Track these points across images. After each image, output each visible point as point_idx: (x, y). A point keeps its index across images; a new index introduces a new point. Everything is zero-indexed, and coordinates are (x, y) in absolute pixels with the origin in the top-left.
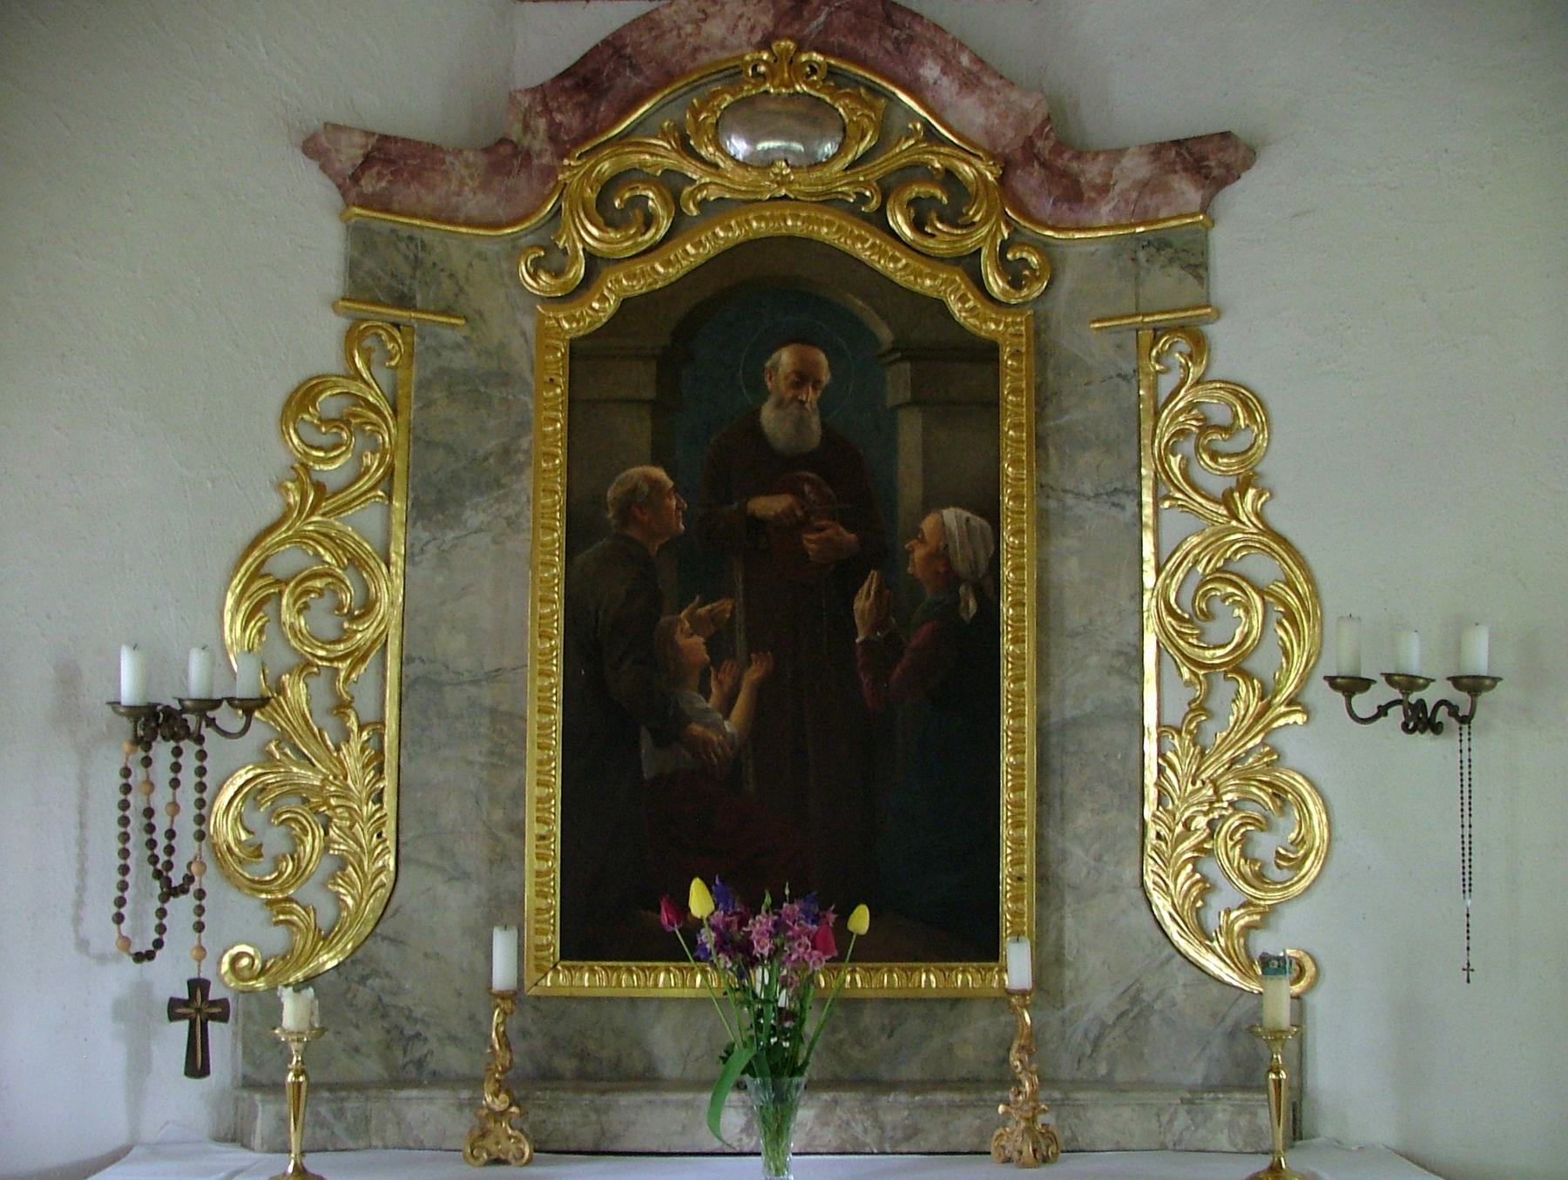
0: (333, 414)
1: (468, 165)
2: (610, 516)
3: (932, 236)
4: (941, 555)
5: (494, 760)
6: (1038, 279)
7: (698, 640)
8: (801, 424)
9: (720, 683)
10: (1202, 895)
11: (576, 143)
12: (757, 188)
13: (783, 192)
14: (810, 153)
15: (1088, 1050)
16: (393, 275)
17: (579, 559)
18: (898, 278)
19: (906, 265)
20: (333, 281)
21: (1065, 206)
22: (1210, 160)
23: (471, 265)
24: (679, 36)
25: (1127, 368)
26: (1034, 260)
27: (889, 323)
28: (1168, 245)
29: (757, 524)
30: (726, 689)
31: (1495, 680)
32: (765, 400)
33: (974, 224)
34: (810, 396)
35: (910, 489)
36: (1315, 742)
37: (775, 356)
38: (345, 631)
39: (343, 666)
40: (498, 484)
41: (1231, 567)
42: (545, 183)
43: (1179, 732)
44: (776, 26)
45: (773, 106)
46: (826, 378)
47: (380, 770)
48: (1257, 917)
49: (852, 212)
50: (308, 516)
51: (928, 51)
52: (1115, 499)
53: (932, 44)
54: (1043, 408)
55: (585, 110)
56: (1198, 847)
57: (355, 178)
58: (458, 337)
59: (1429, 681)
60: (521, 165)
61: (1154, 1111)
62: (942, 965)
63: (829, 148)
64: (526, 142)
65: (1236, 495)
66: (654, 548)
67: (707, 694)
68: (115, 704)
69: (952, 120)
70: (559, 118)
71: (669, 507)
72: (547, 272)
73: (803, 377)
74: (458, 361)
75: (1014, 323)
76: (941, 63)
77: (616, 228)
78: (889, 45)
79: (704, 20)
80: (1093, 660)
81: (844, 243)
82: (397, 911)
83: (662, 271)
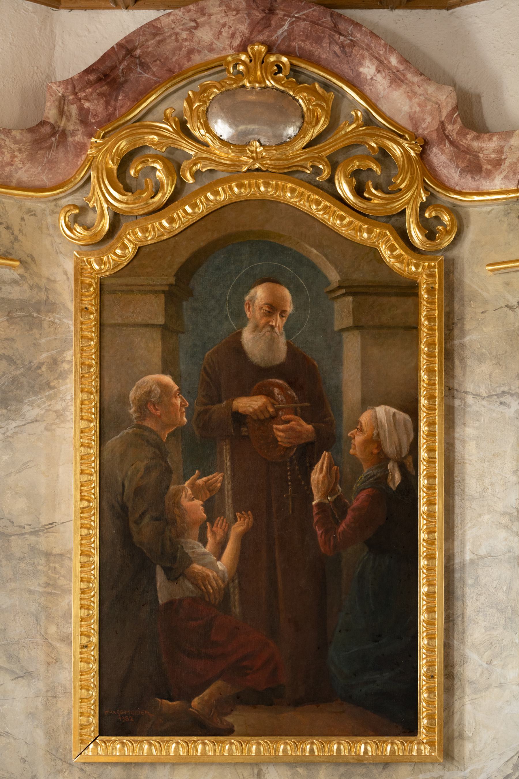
1: (16, 142)
2: (132, 411)
4: (375, 441)
6: (448, 233)
7: (198, 503)
8: (272, 343)
9: (214, 533)
12: (236, 164)
13: (257, 166)
17: (109, 443)
18: (344, 231)
19: (350, 223)
21: (469, 176)
23: (23, 219)
27: (336, 267)
29: (239, 418)
30: (218, 538)
32: (244, 325)
33: (400, 190)
34: (278, 322)
35: (352, 391)
37: (252, 291)
44: (251, 33)
46: (290, 308)
52: (502, 399)
53: (368, 48)
55: (107, 99)
58: (15, 275)
60: (59, 142)
63: (291, 131)
70: (87, 105)
72: (82, 225)
73: (273, 308)
76: (376, 62)
78: (337, 49)
79: (196, 28)
80: (486, 517)
81: (304, 205)
83: (164, 226)
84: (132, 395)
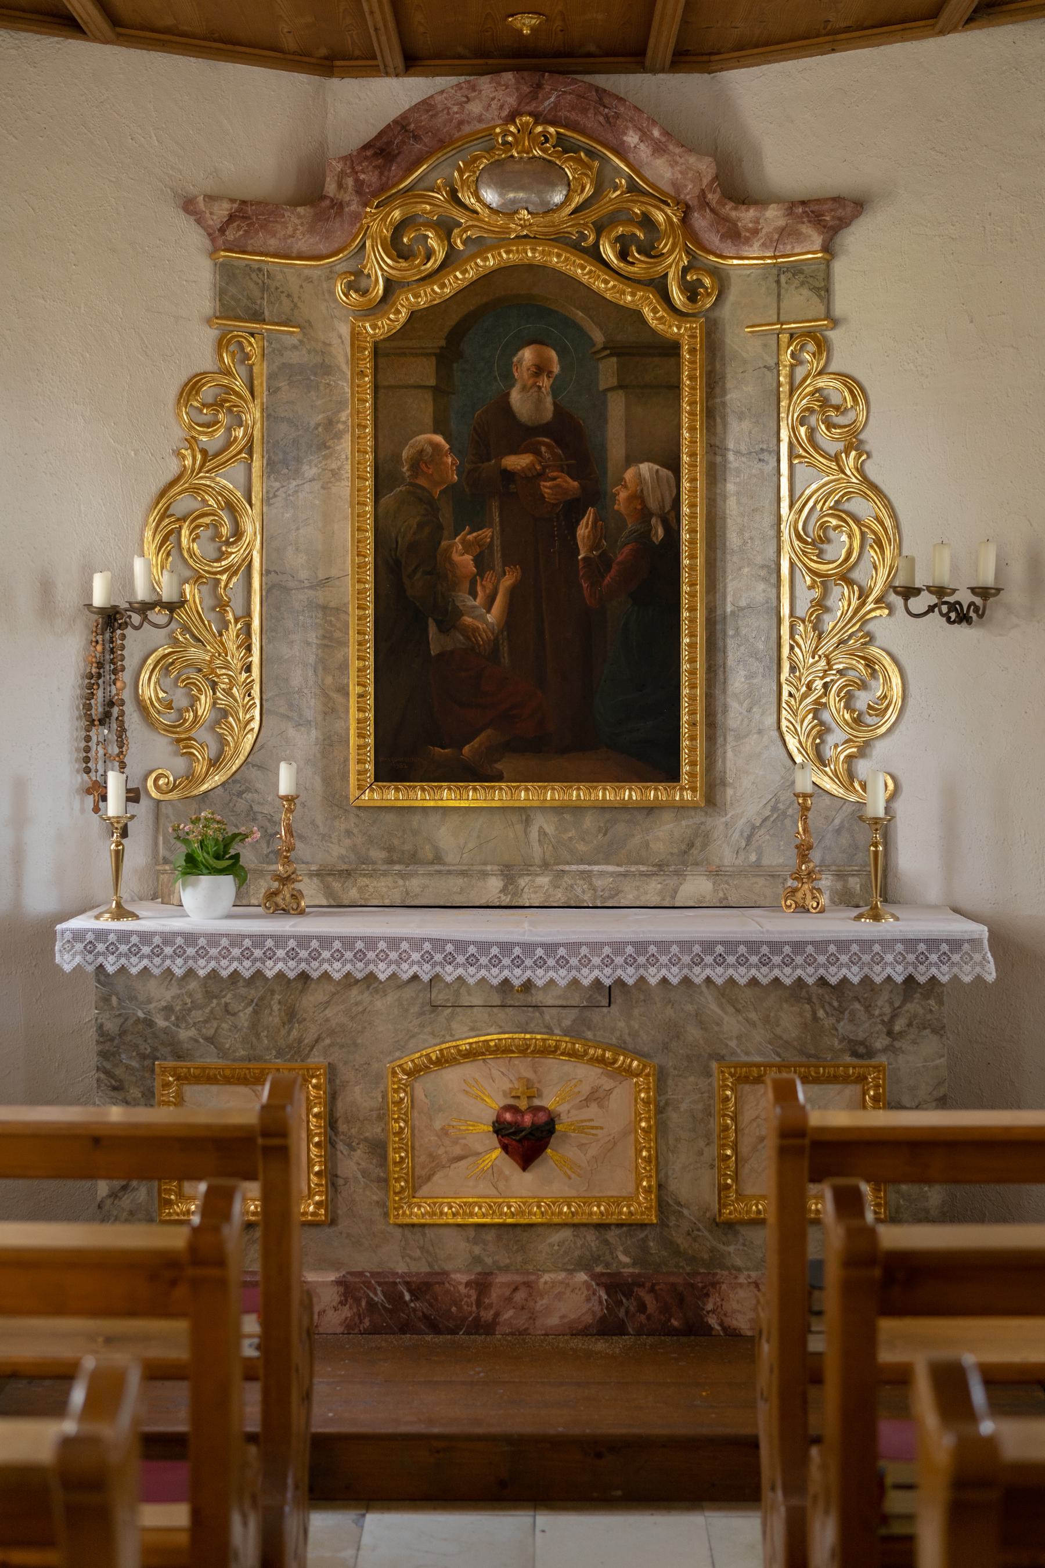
0: (210, 400)
1: (299, 217)
2: (405, 469)
3: (632, 264)
4: (638, 497)
5: (326, 642)
6: (709, 295)
7: (468, 558)
10: (820, 735)
11: (375, 195)
14: (544, 203)
15: (743, 844)
16: (248, 298)
19: (614, 286)
20: (204, 302)
22: (831, 215)
23: (301, 287)
24: (448, 114)
25: (772, 362)
26: (707, 281)
27: (601, 329)
28: (801, 272)
29: (508, 476)
30: (488, 591)
31: (999, 590)
32: (513, 386)
34: (545, 382)
35: (616, 447)
36: (892, 629)
37: (520, 353)
38: (223, 553)
39: (224, 577)
40: (324, 446)
41: (841, 507)
42: (353, 224)
43: (803, 621)
44: (519, 104)
45: (517, 167)
46: (556, 369)
47: (249, 649)
48: (855, 750)
49: (576, 247)
50: (198, 474)
51: (630, 125)
53: (632, 120)
54: (713, 389)
55: (381, 170)
56: (816, 702)
57: (222, 230)
58: (294, 340)
59: (954, 591)
61: (781, 880)
62: (640, 785)
63: (558, 198)
64: (339, 196)
65: (843, 455)
66: (437, 492)
67: (474, 594)
68: (89, 606)
69: (648, 174)
70: (362, 177)
71: (447, 463)
73: (540, 369)
74: (294, 358)
75: (691, 328)
76: (639, 133)
77: (406, 259)
78: (601, 119)
79: (467, 102)
82: (262, 747)
84: (404, 454)
